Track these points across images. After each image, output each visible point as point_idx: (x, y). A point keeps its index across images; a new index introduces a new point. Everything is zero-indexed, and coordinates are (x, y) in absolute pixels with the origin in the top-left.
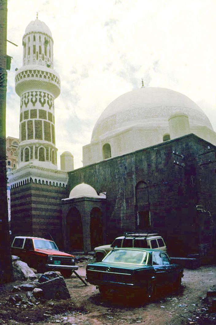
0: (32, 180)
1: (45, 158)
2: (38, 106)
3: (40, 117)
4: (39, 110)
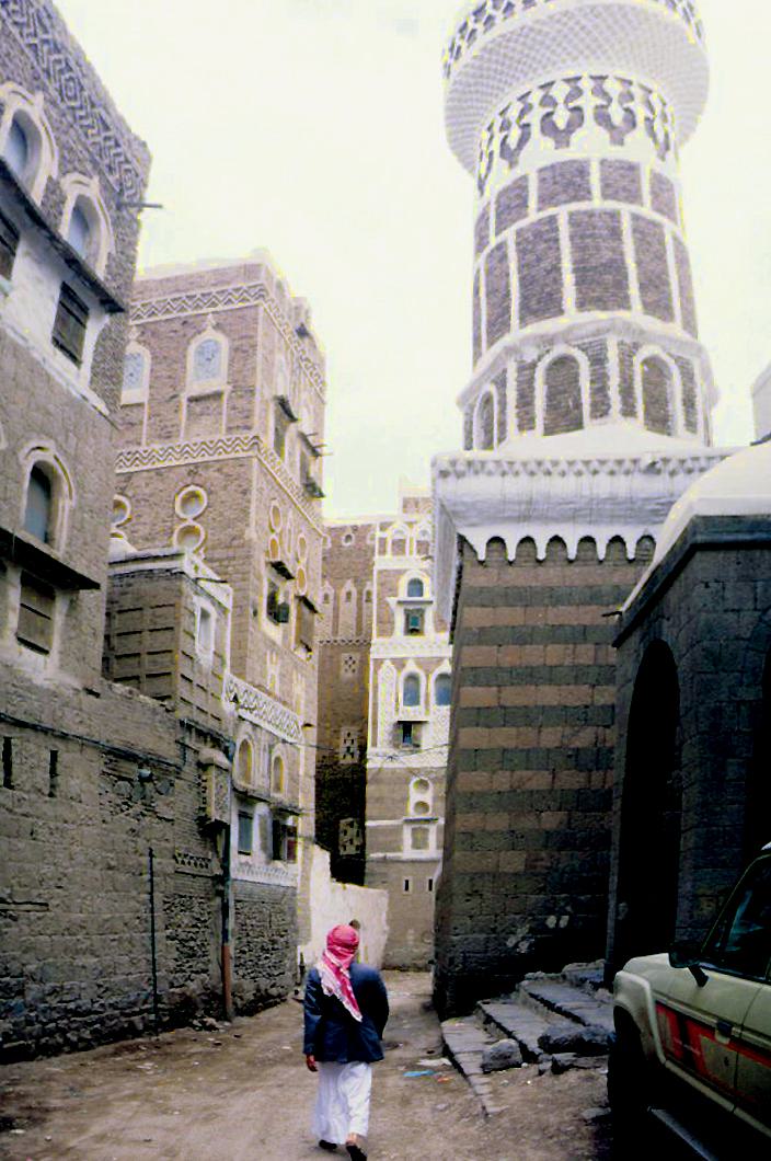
0: (471, 547)
1: (586, 409)
2: (591, 144)
3: (609, 191)
4: (603, 162)
